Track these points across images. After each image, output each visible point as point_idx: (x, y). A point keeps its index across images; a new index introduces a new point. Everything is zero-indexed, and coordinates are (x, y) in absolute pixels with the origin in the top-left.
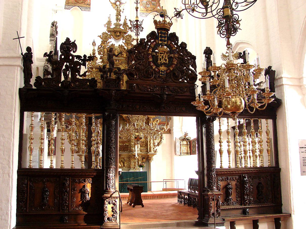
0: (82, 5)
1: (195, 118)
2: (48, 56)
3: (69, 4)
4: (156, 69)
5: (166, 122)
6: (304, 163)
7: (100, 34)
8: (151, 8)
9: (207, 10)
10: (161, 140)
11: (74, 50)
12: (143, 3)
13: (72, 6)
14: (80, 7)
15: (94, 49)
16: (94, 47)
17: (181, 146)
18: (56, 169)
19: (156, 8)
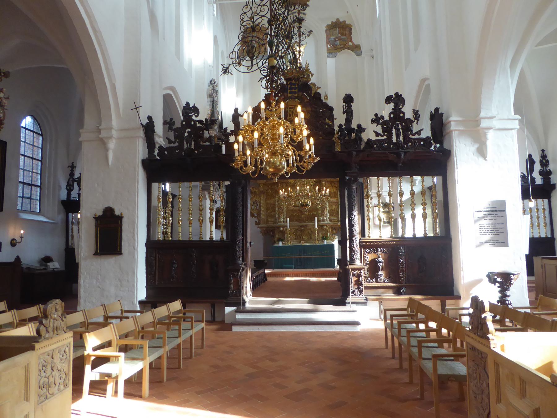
1: (441, 177)
2: (168, 123)
6: (481, 232)
9: (252, 63)
11: (196, 115)
12: (330, 40)
18: (216, 241)
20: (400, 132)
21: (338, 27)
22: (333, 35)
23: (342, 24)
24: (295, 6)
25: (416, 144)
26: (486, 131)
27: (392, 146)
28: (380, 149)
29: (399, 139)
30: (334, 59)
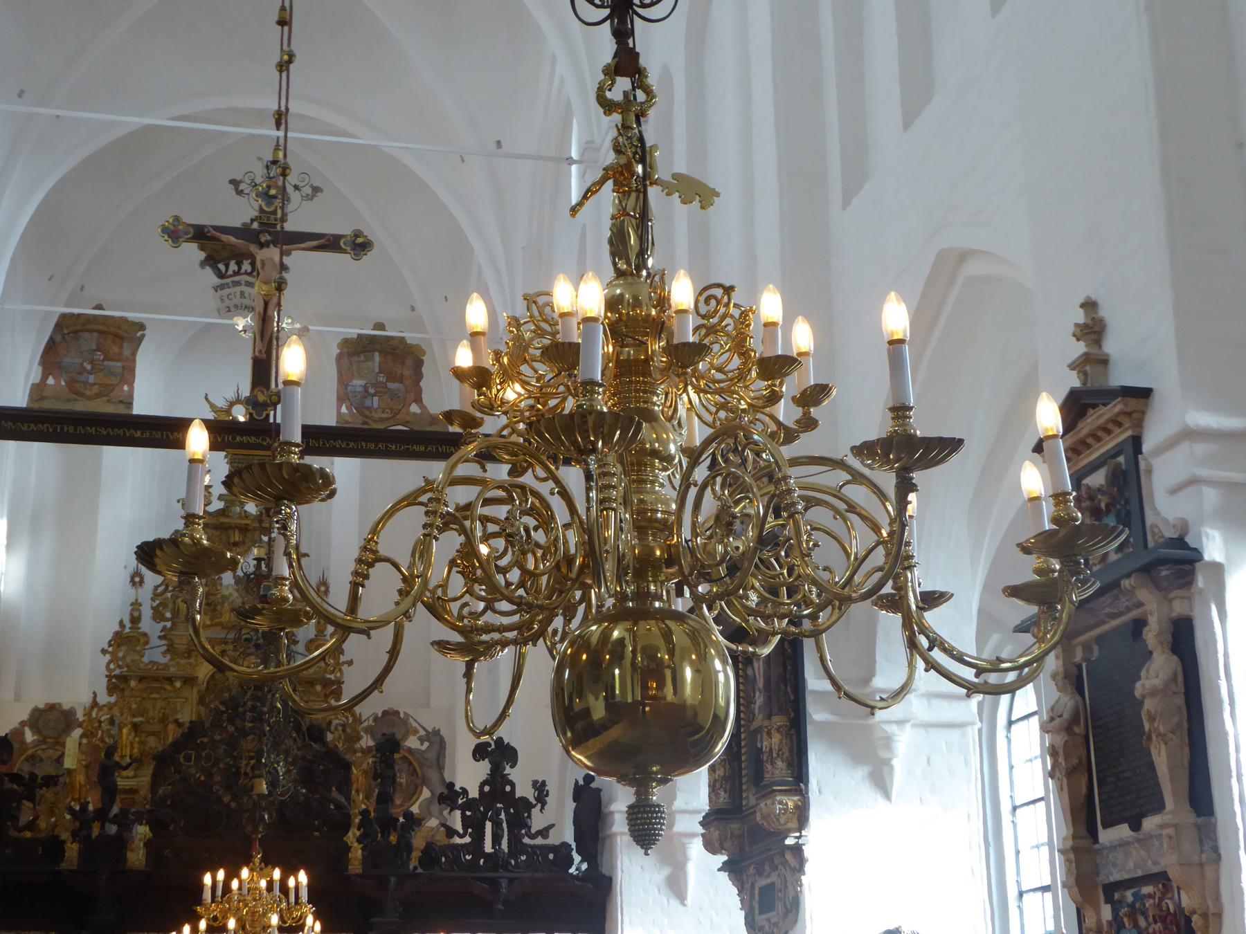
4: (233, 805)
12: (349, 388)
15: (137, 600)
16: (137, 592)
20: (503, 830)
21: (381, 352)
22: (361, 377)
24: (239, 264)
25: (538, 858)
26: (685, 840)
27: (482, 861)
28: (455, 867)
29: (500, 845)
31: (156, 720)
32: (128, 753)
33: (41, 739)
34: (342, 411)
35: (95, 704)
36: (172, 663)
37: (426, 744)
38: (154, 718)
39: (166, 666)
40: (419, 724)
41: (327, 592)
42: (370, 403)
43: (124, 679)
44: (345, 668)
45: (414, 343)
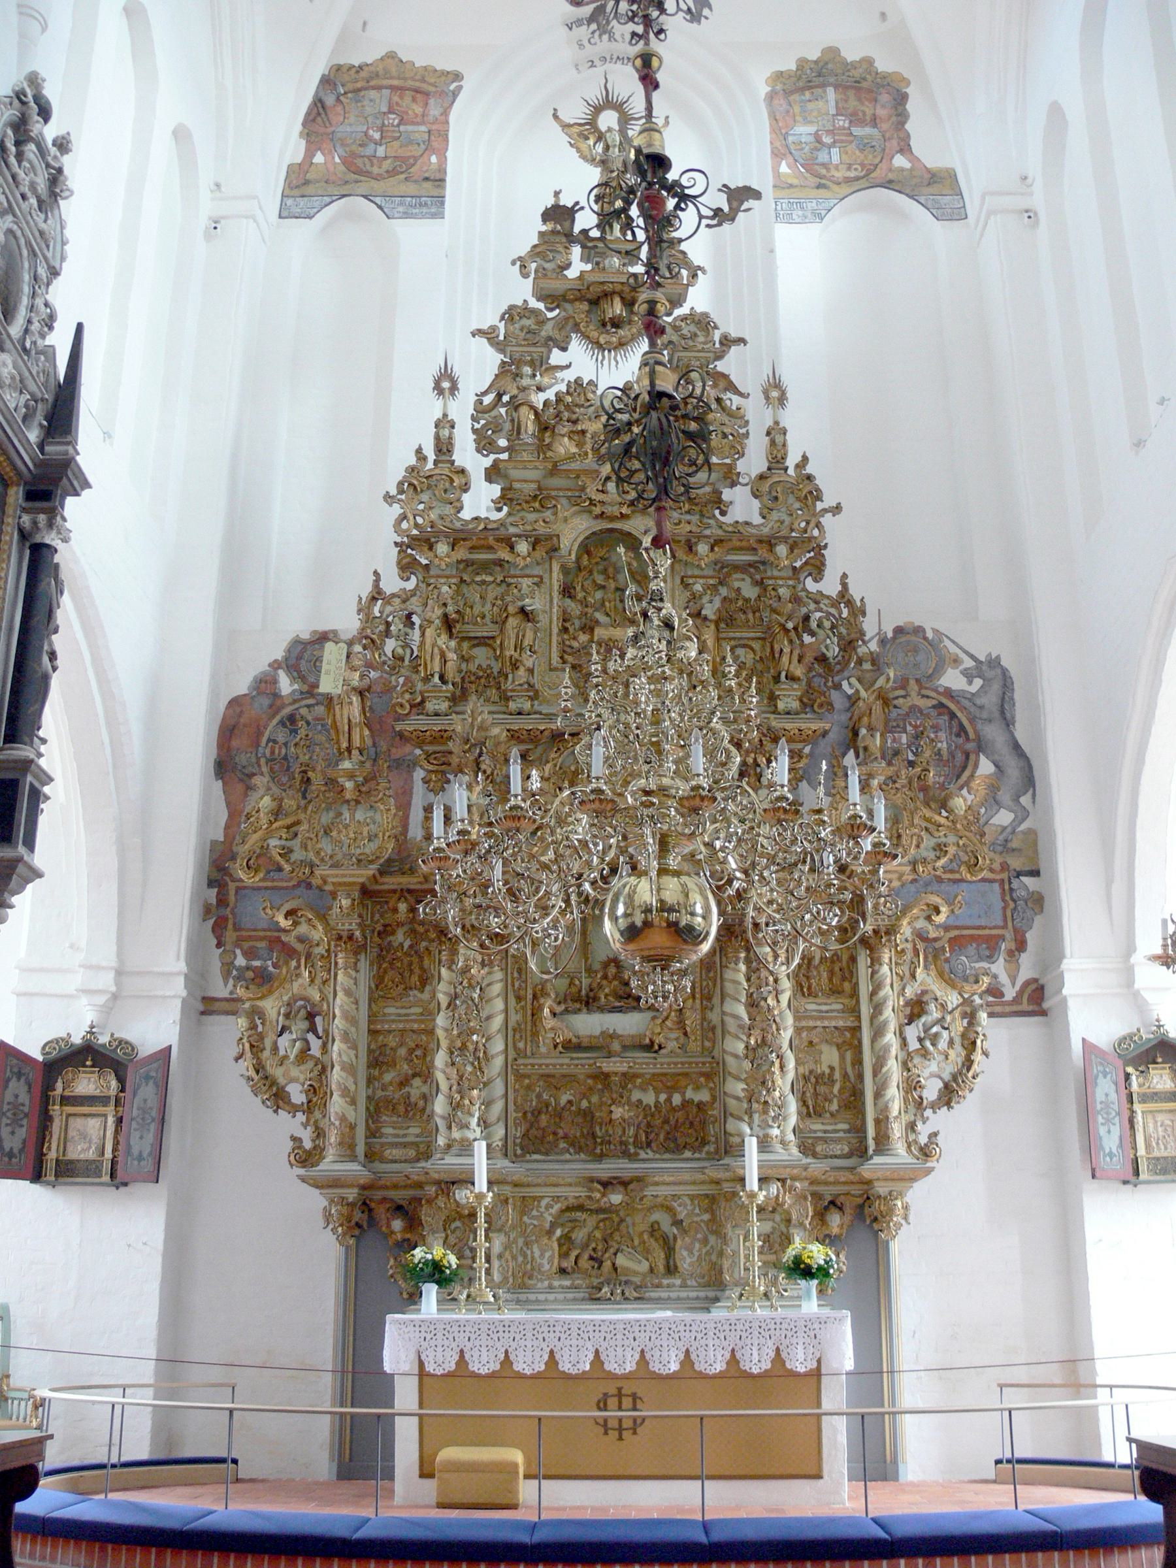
0: (393, 185)
3: (309, 190)
5: (1005, 927)
7: (491, 318)
8: (849, 169)
10: (969, 1063)
12: (790, 139)
13: (327, 199)
14: (378, 200)
15: (445, 415)
16: (445, 405)
17: (1138, 1107)
19: (884, 165)
22: (807, 122)
23: (857, 74)
30: (815, 229)
31: (488, 619)
32: (437, 669)
33: (305, 688)
34: (781, 170)
35: (377, 594)
36: (511, 519)
37: (978, 683)
38: (483, 617)
39: (502, 523)
40: (961, 648)
41: (782, 400)
42: (827, 157)
43: (426, 541)
44: (827, 520)
45: (890, 71)
